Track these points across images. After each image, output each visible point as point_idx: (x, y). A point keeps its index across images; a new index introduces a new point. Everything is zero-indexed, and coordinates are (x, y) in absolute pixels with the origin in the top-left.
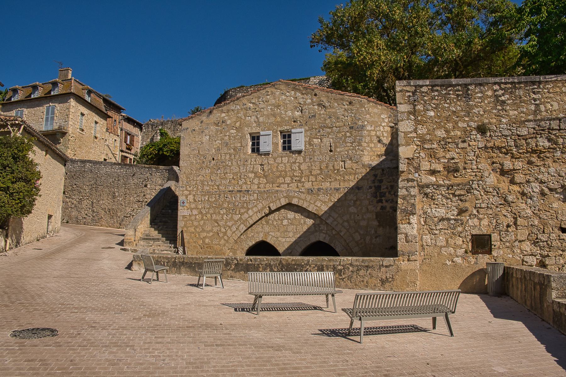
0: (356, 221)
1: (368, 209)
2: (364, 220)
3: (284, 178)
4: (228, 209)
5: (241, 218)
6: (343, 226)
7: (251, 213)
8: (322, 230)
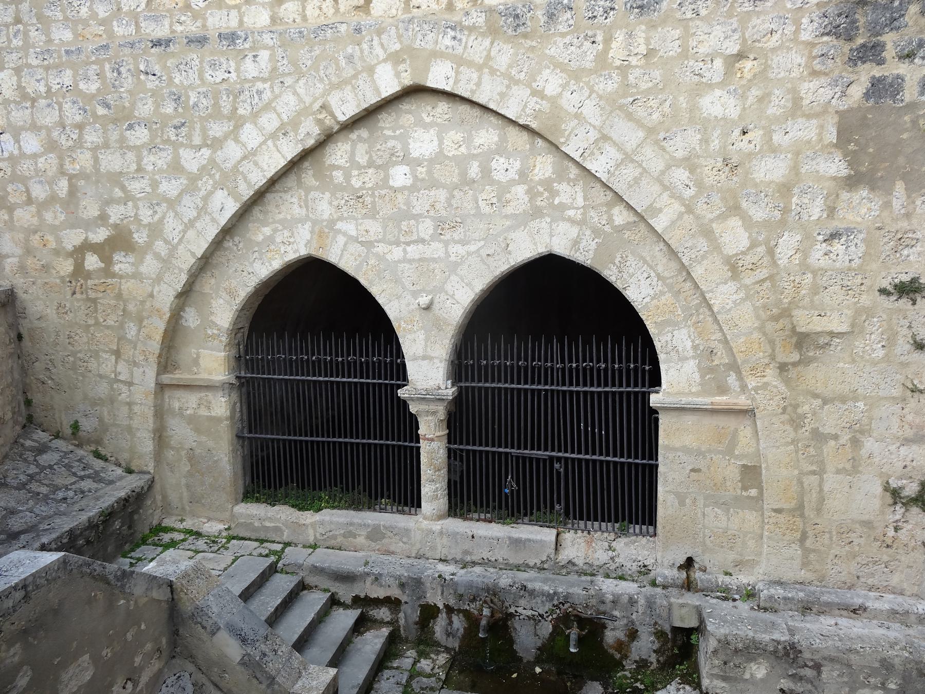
0: (735, 160)
1: (797, 101)
2: (774, 150)
4: (154, 124)
5: (212, 161)
6: (665, 188)
7: (250, 135)
8: (562, 207)
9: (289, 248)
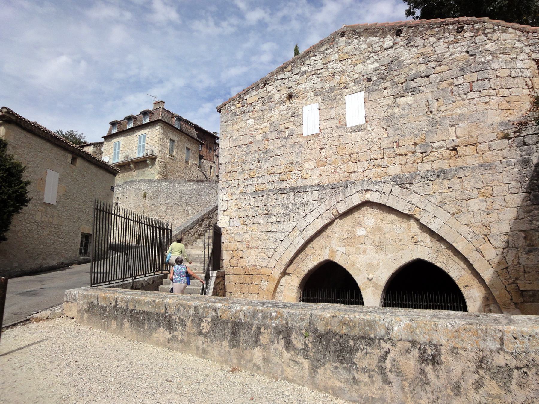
7: (309, 218)
9: (321, 257)
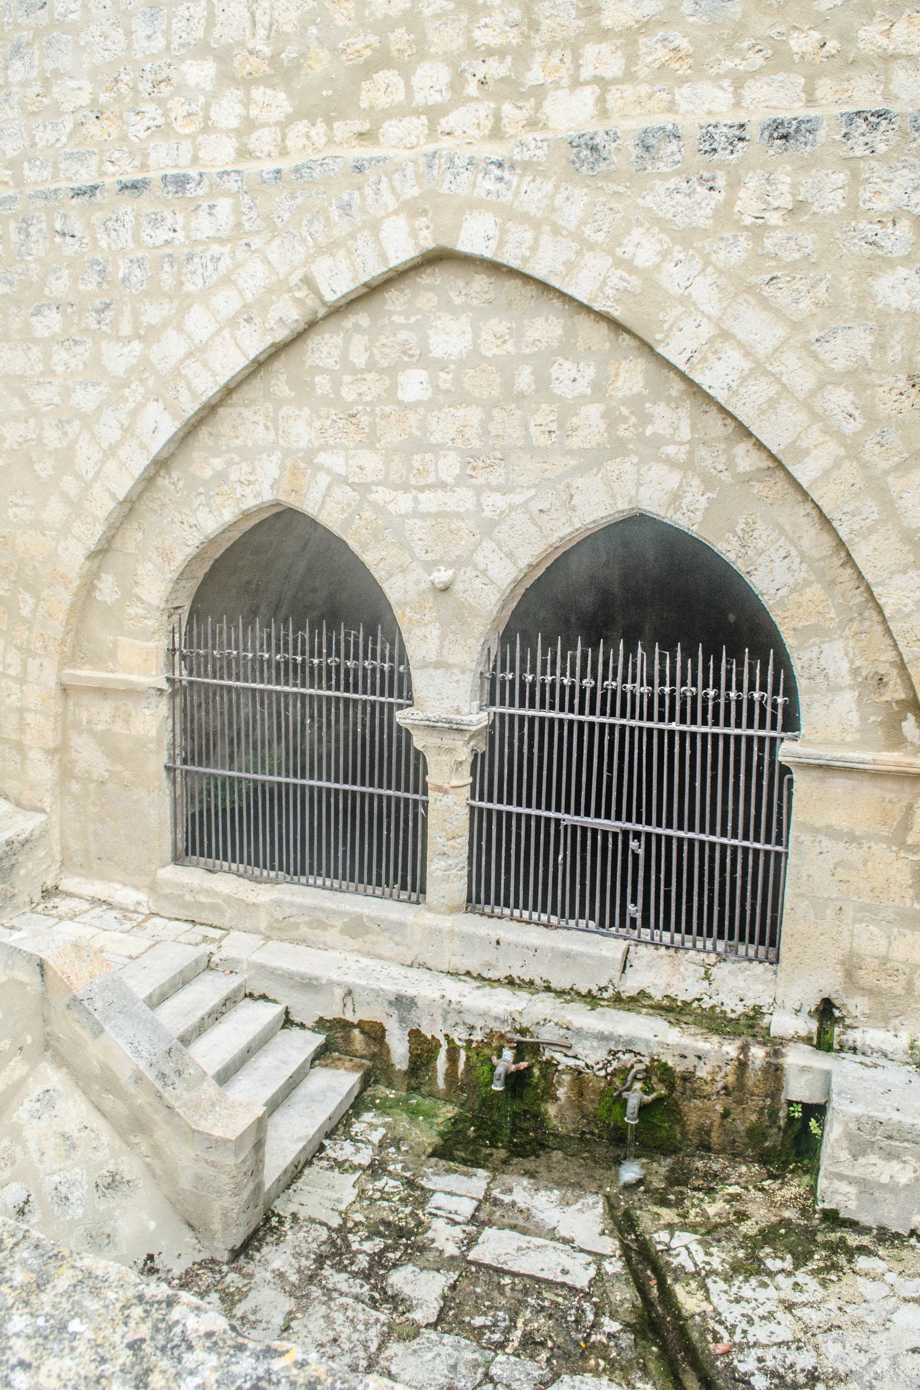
3: (406, 74)
6: (816, 417)
8: (658, 441)
